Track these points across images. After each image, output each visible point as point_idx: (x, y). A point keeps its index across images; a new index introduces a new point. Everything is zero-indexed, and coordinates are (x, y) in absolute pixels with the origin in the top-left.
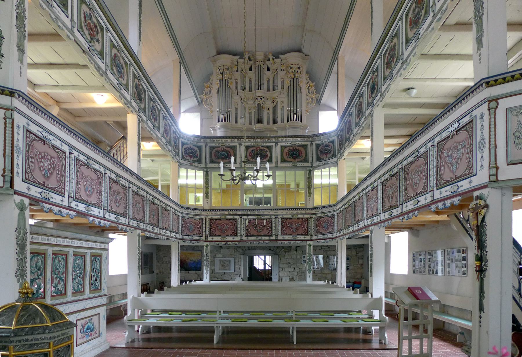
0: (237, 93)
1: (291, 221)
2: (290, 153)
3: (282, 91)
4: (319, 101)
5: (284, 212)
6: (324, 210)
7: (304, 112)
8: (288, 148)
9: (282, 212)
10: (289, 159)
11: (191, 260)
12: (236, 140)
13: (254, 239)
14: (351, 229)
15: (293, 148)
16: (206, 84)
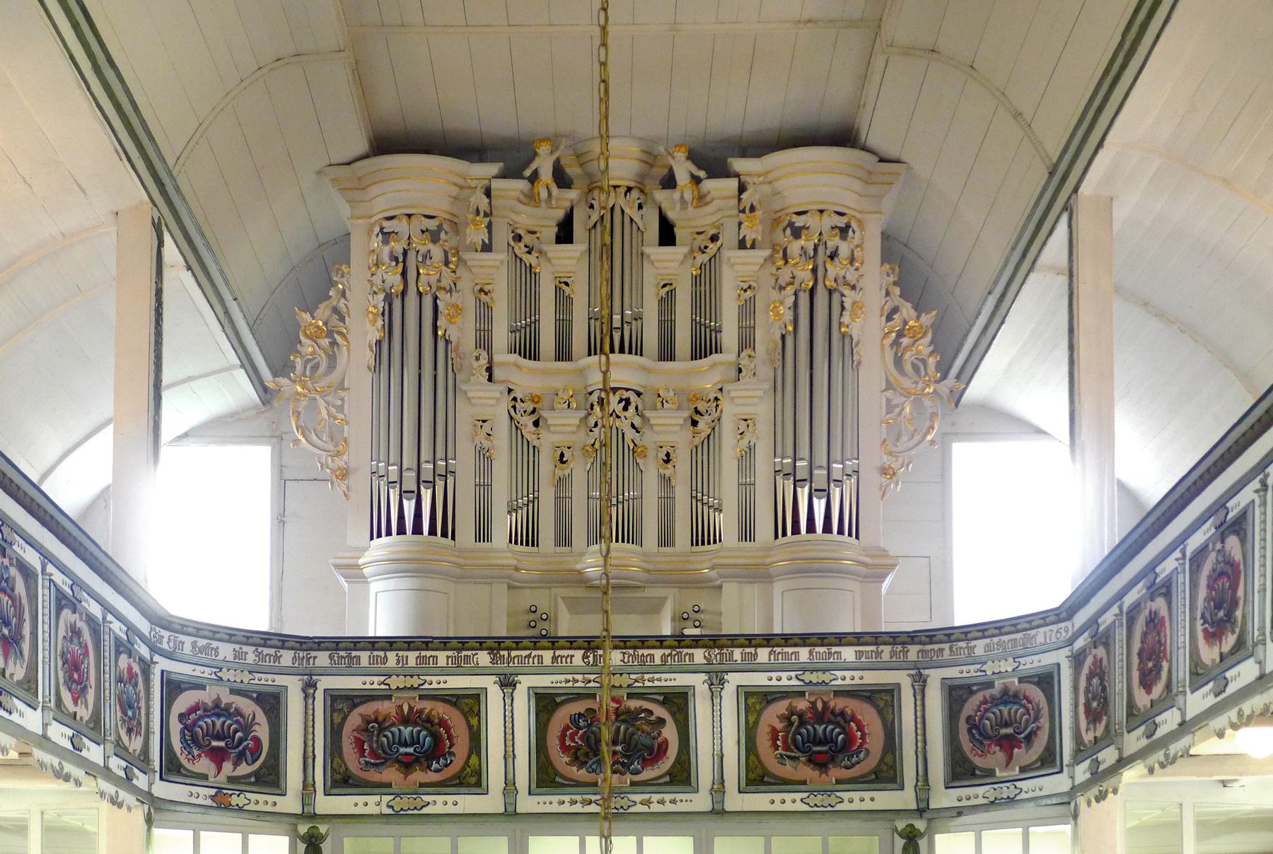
0: (489, 370)
2: (798, 732)
3: (744, 362)
8: (781, 707)
10: (787, 770)
12: (483, 658)
15: (814, 704)
16: (307, 316)
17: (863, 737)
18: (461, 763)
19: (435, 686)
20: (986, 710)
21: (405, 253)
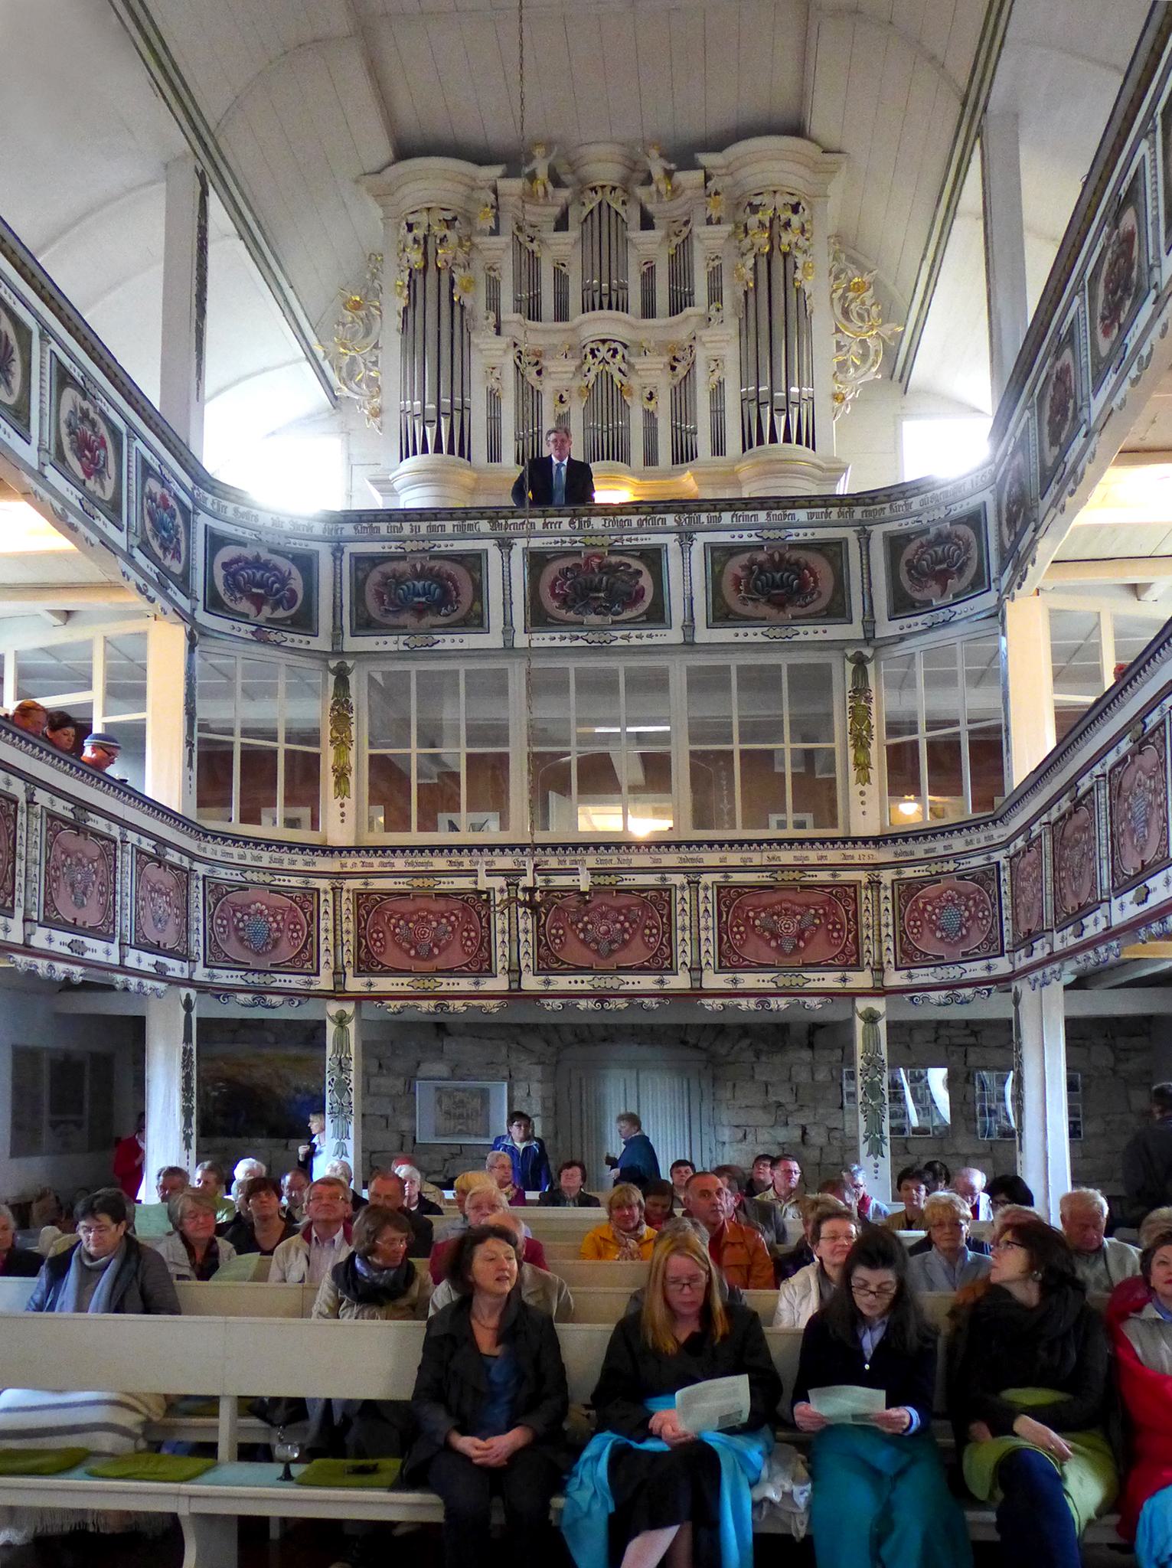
1: (767, 898)
2: (758, 578)
4: (902, 376)
5: (734, 858)
6: (939, 846)
7: (823, 407)
8: (743, 559)
9: (722, 855)
10: (749, 609)
11: (297, 1090)
12: (484, 526)
13: (580, 986)
14: (1094, 926)
15: (771, 556)
17: (816, 582)
18: (466, 609)
19: (443, 548)
20: (923, 553)
21: (425, 238)
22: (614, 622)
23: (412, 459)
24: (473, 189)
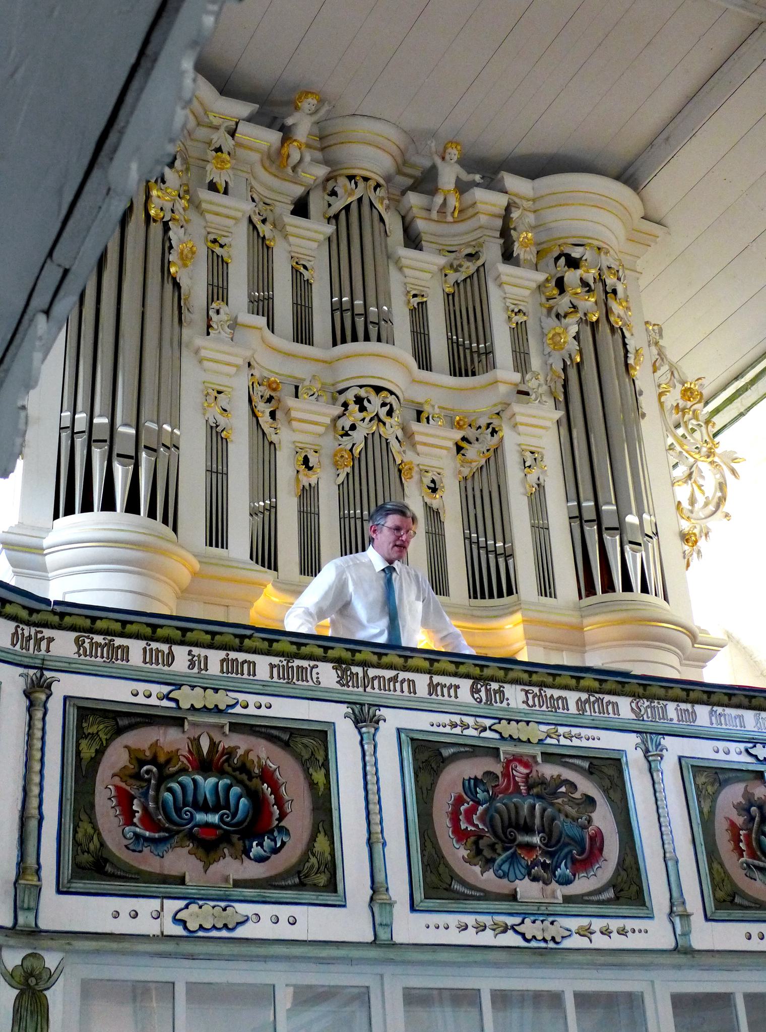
22: (568, 899)
23: (79, 517)
24: (199, 124)
